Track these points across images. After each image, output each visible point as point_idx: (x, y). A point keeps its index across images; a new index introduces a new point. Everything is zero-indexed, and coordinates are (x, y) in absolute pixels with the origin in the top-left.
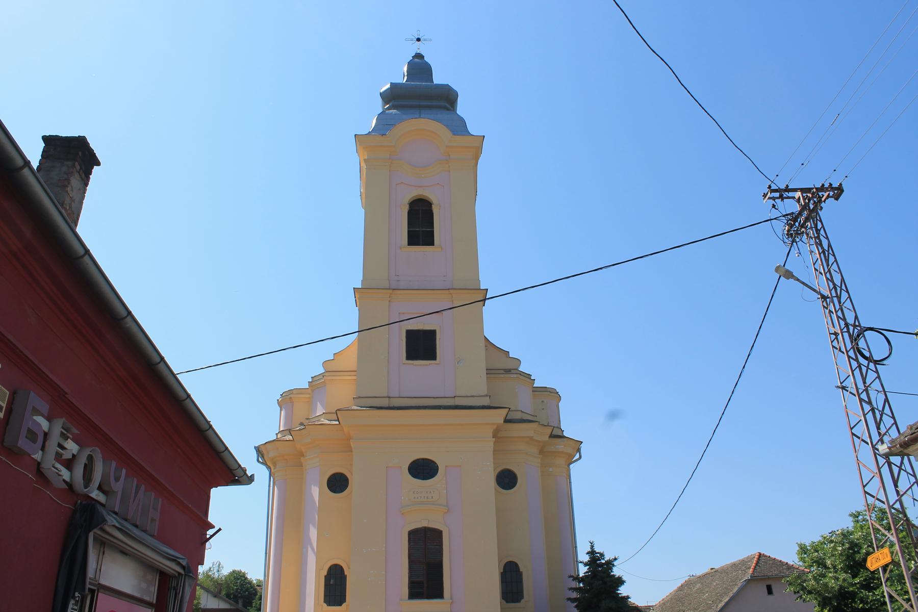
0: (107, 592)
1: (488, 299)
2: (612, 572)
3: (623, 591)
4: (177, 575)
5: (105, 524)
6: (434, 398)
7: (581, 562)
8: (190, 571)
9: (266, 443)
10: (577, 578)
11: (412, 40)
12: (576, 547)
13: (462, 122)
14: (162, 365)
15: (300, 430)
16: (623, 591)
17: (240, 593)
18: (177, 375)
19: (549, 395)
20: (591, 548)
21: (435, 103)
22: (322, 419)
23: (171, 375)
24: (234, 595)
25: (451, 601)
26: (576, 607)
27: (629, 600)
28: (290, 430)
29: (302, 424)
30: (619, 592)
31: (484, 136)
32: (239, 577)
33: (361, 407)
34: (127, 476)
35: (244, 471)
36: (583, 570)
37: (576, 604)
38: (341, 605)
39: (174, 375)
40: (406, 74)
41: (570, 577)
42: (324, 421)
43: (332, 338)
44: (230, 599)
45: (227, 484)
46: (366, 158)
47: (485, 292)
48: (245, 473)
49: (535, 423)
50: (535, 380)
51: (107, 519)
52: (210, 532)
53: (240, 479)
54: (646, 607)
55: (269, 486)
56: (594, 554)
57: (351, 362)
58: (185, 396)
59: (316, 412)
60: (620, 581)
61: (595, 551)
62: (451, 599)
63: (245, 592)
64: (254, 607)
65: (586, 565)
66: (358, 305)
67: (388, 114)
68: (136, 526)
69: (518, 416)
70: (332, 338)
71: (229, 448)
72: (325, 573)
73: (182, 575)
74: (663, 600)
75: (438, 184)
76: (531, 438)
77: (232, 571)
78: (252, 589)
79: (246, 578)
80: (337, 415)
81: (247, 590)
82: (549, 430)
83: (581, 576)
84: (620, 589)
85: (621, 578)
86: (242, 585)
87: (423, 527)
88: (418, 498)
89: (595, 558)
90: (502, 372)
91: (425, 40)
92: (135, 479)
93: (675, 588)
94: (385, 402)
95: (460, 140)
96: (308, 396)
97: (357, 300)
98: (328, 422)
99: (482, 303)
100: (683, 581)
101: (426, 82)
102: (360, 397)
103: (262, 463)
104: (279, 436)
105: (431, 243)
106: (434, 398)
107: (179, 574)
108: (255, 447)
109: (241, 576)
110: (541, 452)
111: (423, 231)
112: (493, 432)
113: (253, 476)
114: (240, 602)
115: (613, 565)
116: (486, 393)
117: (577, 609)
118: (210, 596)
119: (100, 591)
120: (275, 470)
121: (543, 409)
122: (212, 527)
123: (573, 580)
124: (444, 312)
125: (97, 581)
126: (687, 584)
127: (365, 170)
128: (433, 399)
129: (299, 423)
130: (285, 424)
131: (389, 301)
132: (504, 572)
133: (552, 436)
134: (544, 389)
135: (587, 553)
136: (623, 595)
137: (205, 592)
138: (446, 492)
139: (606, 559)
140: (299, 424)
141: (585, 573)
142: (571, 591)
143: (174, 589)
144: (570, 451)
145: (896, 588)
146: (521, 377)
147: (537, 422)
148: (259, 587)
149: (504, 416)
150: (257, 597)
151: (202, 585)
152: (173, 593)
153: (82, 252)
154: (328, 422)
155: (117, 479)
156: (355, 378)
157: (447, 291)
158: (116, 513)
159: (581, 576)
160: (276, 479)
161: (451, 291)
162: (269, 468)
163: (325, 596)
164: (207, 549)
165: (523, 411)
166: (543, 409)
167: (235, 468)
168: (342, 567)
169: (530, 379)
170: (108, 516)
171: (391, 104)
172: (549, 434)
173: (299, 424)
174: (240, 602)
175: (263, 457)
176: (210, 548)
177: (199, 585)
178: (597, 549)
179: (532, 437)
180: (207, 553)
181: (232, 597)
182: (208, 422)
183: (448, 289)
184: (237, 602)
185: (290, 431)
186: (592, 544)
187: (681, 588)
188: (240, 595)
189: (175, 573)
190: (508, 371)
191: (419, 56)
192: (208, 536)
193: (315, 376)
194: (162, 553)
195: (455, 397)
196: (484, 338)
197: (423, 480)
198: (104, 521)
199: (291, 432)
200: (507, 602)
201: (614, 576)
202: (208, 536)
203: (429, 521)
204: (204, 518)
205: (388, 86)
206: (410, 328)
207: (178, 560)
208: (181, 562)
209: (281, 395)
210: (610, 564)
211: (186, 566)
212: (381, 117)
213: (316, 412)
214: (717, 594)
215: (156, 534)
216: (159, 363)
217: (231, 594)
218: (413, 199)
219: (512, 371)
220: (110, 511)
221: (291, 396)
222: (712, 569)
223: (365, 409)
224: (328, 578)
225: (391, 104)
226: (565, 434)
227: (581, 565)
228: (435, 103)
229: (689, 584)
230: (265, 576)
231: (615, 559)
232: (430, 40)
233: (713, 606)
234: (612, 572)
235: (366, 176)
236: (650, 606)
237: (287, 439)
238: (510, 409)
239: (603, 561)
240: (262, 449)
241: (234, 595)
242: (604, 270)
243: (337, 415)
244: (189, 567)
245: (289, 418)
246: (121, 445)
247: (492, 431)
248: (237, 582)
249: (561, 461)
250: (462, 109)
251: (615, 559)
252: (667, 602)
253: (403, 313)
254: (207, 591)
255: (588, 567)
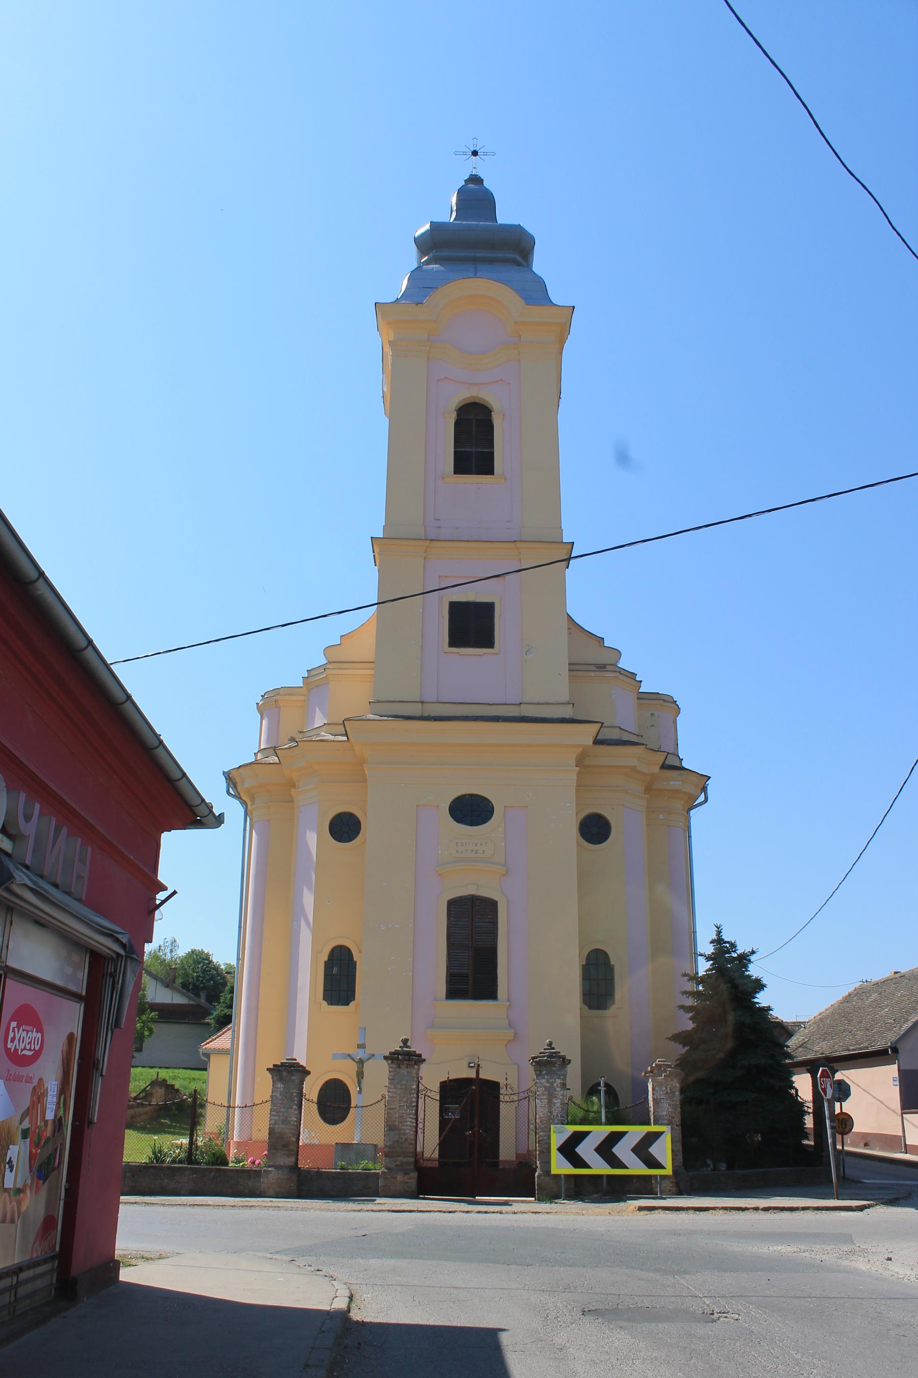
0: (17, 978)
1: (573, 558)
2: (747, 971)
3: (762, 999)
4: (115, 956)
5: (12, 883)
6: (489, 704)
7: (701, 955)
8: (133, 952)
9: (240, 766)
10: (695, 978)
11: (464, 153)
12: (695, 932)
13: (540, 284)
14: (89, 652)
15: (290, 748)
16: (762, 999)
17: (202, 982)
18: (111, 666)
19: (662, 705)
20: (717, 935)
21: (499, 255)
22: (323, 733)
23: (103, 666)
24: (194, 985)
25: (509, 1003)
26: (691, 1019)
27: (771, 1012)
28: (275, 749)
29: (292, 739)
30: (756, 1000)
31: (574, 307)
32: (200, 960)
33: (381, 716)
34: (41, 813)
35: (210, 808)
36: (703, 967)
37: (691, 1014)
38: (347, 1004)
39: (107, 666)
40: (455, 208)
41: (685, 975)
42: (325, 736)
43: (340, 613)
44: (188, 990)
45: (184, 827)
46: (392, 339)
47: (570, 547)
48: (211, 812)
49: (642, 746)
50: (641, 681)
51: (15, 875)
52: (161, 896)
53: (204, 820)
54: (794, 1023)
55: (245, 830)
56: (720, 944)
57: (367, 648)
58: (124, 698)
59: (314, 725)
60: (759, 986)
61: (723, 940)
62: (508, 1001)
63: (209, 981)
64: (223, 1002)
65: (708, 958)
66: (377, 564)
67: (427, 271)
68: (56, 886)
69: (615, 735)
70: (340, 613)
71: (187, 774)
72: (325, 957)
73: (122, 956)
74: (820, 1014)
75: (502, 380)
76: (633, 768)
77: (190, 951)
78: (219, 978)
79: (211, 962)
80: (344, 726)
81: (212, 978)
82: (660, 758)
83: (700, 974)
84: (757, 995)
85: (760, 980)
86: (204, 971)
87: (469, 895)
88: (462, 852)
89: (722, 947)
90: (593, 668)
91: (485, 154)
92: (53, 818)
93: (840, 997)
94: (416, 710)
95: (537, 313)
96: (302, 698)
97: (377, 557)
98: (332, 738)
99: (564, 563)
100: (851, 989)
101: (486, 220)
102: (378, 702)
103: (234, 796)
104: (259, 756)
105: (490, 471)
106: (489, 704)
107: (118, 954)
108: (224, 773)
109: (204, 959)
110: (648, 789)
111: (475, 451)
112: (576, 758)
113: (222, 815)
114: (203, 995)
115: (749, 961)
116: (568, 699)
117: (693, 1023)
118: (159, 985)
119: (8, 976)
120: (253, 807)
121: (653, 726)
122: (164, 888)
123: (689, 980)
124: (507, 577)
125: (3, 962)
126: (857, 993)
127: (389, 357)
128: (487, 706)
129: (289, 738)
130: (269, 739)
131: (425, 558)
132: (586, 964)
133: (664, 767)
134: (655, 697)
135: (711, 942)
136: (762, 1005)
137: (153, 979)
138: (505, 844)
139: (738, 952)
140: (289, 740)
141: (706, 971)
142: (685, 996)
143: (111, 975)
144: (690, 789)
145: (289, 1092)
146: (622, 677)
147: (643, 744)
148: (228, 975)
149: (594, 734)
150: (227, 988)
151: (149, 969)
152: (109, 982)
153: (84, 643)
154: (332, 738)
155: (28, 818)
156: (371, 672)
157: (514, 544)
158: (27, 867)
159: (700, 974)
160: (254, 820)
161: (519, 545)
162: (244, 803)
163: (325, 991)
164: (157, 921)
165: (621, 727)
166: (653, 726)
167: (196, 805)
168: (349, 950)
169: (635, 680)
170: (17, 871)
171: (431, 255)
172: (661, 763)
173: (289, 740)
174: (203, 995)
175: (235, 787)
176: (161, 919)
177: (144, 969)
178: (726, 937)
179: (636, 766)
180: (158, 927)
181: (191, 987)
182: (157, 736)
183: (515, 541)
184: (198, 995)
185: (275, 750)
186: (718, 928)
187: (848, 999)
188: (202, 985)
189: (111, 953)
190: (602, 667)
191: (475, 180)
192: (158, 902)
193: (312, 669)
194: (94, 925)
195: (521, 703)
196: (566, 615)
197: (471, 826)
198: (11, 877)
199: (277, 751)
200: (590, 1007)
201: (749, 976)
202: (158, 902)
203: (478, 886)
204: (151, 875)
205: (427, 227)
206: (455, 599)
207: (116, 935)
208: (120, 938)
209: (262, 696)
210: (744, 959)
211: (127, 944)
212: (415, 276)
213: (314, 724)
214: (902, 1009)
215: (84, 898)
216: (86, 648)
217: (190, 984)
218: (465, 403)
219: (608, 668)
220: (20, 864)
221: (278, 697)
222: (896, 973)
223: (386, 718)
224: (329, 965)
225: (431, 255)
226: (685, 764)
227: (701, 960)
228: (499, 255)
229: (860, 993)
230: (238, 959)
231: (753, 952)
232: (494, 154)
233: (895, 1027)
234: (747, 971)
235: (392, 367)
236: (800, 1022)
237: (271, 762)
238: (602, 724)
239: (735, 955)
240: (235, 775)
241: (194, 985)
242: (754, 517)
243: (344, 726)
244: (131, 945)
245: (273, 731)
246: (33, 768)
247: (575, 756)
248: (198, 968)
249: (678, 805)
250: (540, 264)
251: (753, 952)
252: (827, 1017)
253: (446, 577)
254: (155, 979)
255: (711, 962)
